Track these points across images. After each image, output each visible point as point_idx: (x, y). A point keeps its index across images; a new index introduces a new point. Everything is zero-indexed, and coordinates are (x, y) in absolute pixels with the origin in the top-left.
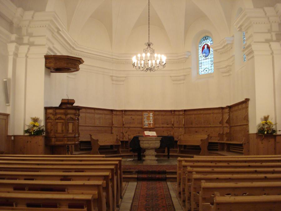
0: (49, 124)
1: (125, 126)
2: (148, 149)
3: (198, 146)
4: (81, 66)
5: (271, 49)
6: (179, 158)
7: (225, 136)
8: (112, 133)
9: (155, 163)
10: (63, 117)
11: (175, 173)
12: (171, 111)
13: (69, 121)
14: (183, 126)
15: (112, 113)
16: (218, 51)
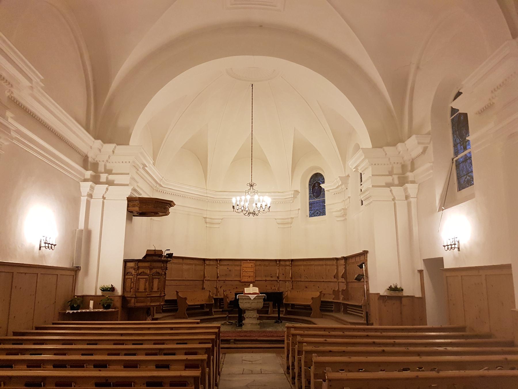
0: (129, 281)
1: (219, 279)
2: (248, 310)
3: (309, 306)
4: (171, 209)
5: (392, 194)
6: (288, 324)
7: (340, 293)
8: (203, 289)
9: (256, 328)
10: (148, 271)
11: (282, 341)
12: (276, 260)
13: (155, 277)
14: (290, 280)
15: (205, 263)
16: (331, 191)
